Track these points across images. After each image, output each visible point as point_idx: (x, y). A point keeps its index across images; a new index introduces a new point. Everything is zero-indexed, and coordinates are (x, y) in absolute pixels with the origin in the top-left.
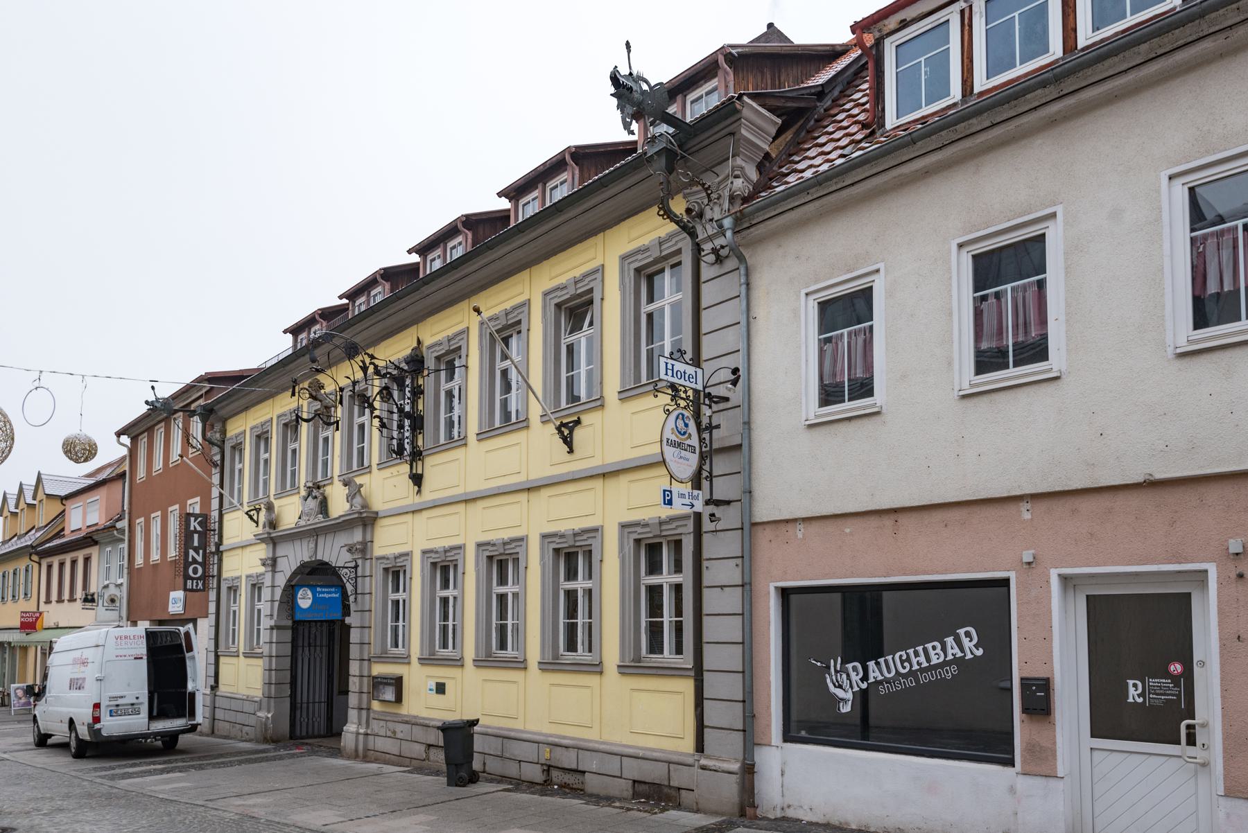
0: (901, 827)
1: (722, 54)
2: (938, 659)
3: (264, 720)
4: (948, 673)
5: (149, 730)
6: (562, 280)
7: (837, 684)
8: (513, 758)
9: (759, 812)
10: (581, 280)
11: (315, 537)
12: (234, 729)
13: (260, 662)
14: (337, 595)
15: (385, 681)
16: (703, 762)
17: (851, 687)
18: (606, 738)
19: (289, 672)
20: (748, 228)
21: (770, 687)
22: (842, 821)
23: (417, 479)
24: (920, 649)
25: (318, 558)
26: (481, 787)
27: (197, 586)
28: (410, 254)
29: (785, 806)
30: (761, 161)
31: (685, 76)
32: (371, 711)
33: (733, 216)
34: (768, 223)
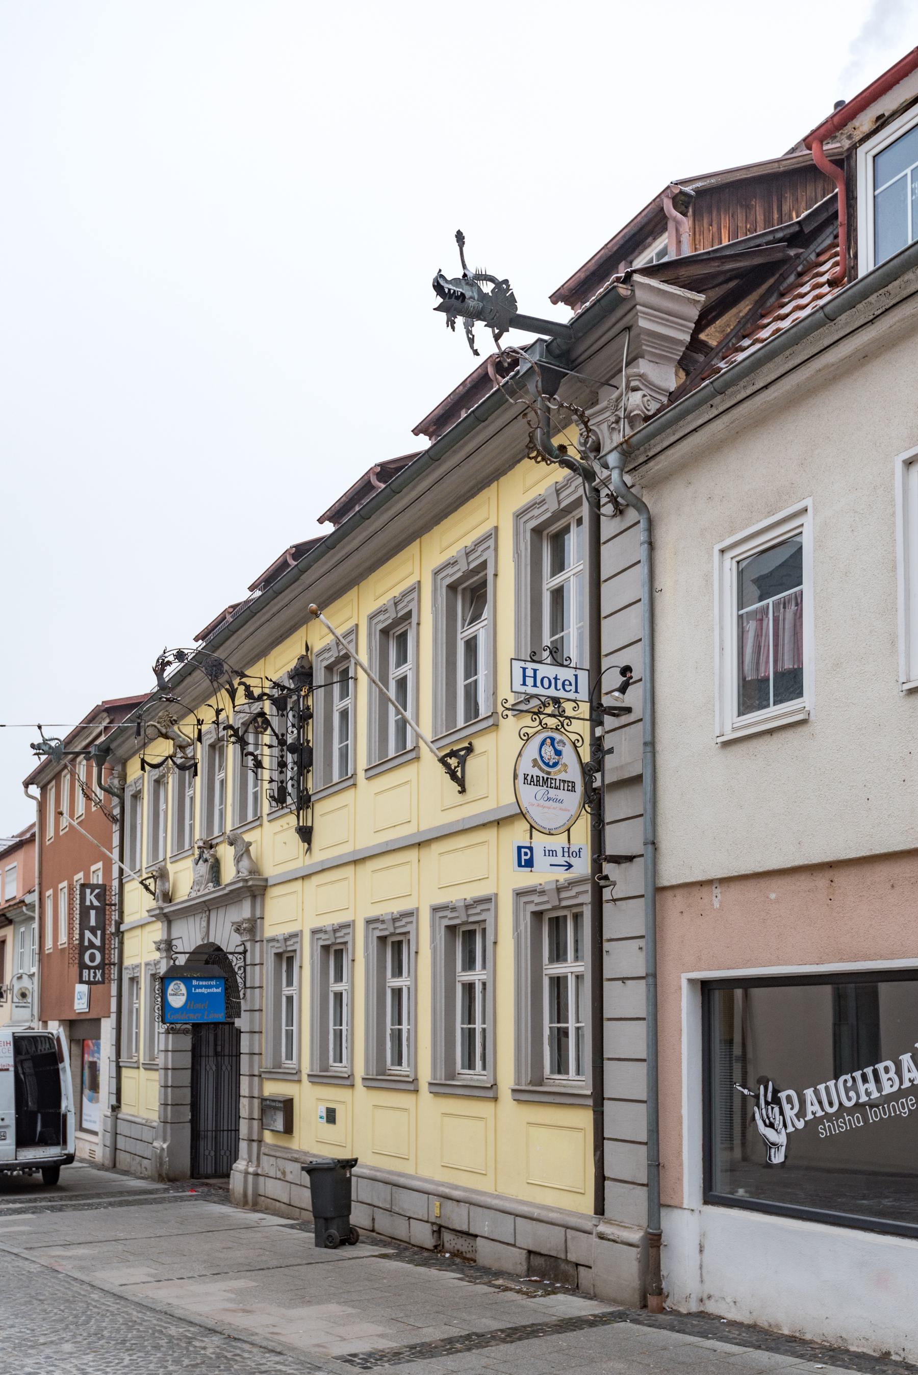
0: (844, 1336)
1: (667, 197)
2: (891, 1086)
3: (159, 1151)
4: (904, 1109)
5: (16, 1159)
6: (453, 552)
7: (767, 1121)
8: (402, 1213)
9: (667, 1305)
10: (473, 551)
11: (208, 912)
12: (134, 1162)
13: (155, 1076)
14: (219, 990)
15: (273, 1104)
16: (602, 1228)
17: (785, 1126)
18: (502, 1190)
19: (189, 1089)
20: (646, 462)
21: (681, 1123)
22: (772, 1321)
23: (306, 834)
24: (869, 1071)
25: (210, 941)
26: (363, 1250)
27: (95, 977)
28: (321, 523)
29: (705, 1297)
30: (684, 353)
31: (624, 236)
32: (263, 1143)
33: (619, 449)
34: (670, 452)
